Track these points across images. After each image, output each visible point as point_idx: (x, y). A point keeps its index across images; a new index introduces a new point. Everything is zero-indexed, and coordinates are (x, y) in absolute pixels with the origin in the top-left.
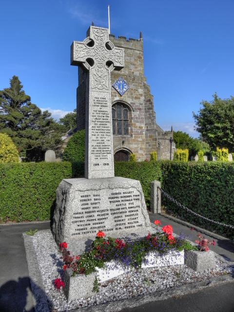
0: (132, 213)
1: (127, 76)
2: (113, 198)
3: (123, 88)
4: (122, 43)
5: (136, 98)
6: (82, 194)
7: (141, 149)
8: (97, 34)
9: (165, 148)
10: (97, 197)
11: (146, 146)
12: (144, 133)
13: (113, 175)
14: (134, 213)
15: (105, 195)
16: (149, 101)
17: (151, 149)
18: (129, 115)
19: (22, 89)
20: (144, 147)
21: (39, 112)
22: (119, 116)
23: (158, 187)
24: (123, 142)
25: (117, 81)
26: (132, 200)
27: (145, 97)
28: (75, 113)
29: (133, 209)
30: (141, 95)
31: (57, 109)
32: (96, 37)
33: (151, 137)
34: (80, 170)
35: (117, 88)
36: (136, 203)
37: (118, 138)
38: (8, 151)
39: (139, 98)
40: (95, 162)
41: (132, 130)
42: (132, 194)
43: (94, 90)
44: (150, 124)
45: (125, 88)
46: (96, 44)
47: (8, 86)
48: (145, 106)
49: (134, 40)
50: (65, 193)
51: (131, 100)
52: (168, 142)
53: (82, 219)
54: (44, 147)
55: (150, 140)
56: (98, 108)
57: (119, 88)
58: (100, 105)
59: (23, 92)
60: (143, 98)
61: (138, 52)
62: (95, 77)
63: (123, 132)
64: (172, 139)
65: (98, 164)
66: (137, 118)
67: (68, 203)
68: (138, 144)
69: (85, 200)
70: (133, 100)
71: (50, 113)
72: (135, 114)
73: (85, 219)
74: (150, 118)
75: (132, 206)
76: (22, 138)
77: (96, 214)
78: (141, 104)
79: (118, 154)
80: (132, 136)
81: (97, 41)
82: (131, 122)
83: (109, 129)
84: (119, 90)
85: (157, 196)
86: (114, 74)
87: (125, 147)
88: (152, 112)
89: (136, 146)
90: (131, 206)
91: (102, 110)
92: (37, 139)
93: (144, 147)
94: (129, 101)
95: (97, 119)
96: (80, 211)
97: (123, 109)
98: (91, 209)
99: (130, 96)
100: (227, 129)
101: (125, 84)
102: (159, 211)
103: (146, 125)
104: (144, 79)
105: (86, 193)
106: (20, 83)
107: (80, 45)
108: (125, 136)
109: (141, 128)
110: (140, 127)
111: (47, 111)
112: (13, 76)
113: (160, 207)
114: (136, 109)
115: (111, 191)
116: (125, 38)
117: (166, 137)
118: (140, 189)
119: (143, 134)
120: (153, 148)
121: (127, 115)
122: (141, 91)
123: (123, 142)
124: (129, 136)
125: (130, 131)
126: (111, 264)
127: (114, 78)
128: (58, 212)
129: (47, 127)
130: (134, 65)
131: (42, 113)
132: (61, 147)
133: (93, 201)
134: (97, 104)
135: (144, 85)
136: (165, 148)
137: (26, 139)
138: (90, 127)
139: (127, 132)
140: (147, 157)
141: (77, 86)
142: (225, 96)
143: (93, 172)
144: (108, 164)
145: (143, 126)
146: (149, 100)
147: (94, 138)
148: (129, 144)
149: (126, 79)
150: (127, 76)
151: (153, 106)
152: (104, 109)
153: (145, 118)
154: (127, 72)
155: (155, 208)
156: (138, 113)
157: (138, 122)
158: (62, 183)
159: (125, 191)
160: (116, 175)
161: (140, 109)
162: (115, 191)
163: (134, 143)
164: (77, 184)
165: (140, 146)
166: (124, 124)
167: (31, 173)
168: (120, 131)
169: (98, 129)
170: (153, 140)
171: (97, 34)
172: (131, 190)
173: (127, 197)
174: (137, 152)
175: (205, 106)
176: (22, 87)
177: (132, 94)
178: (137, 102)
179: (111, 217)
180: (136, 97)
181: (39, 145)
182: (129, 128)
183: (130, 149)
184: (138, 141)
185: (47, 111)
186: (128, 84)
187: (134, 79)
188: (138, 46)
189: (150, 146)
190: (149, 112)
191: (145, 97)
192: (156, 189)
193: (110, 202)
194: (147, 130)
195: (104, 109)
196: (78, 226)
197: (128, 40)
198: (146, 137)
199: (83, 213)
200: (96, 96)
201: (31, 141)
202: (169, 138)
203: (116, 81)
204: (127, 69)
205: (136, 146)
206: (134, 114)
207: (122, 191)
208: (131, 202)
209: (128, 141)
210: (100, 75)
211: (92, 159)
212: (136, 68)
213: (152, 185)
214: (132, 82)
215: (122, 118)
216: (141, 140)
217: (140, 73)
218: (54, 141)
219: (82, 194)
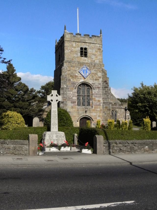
1: (89, 64)
2: (57, 136)
3: (86, 73)
4: (87, 39)
5: (96, 80)
6: (49, 135)
7: (99, 116)
9: (121, 115)
11: (103, 114)
12: (101, 105)
13: (58, 131)
15: (55, 136)
16: (106, 82)
17: (106, 116)
18: (90, 92)
20: (101, 115)
21: (28, 89)
22: (84, 92)
23: (76, 136)
24: (86, 112)
25: (82, 68)
27: (103, 78)
28: (54, 81)
30: (100, 77)
31: (36, 74)
33: (106, 108)
34: (49, 129)
35: (82, 73)
36: (63, 138)
37: (83, 108)
38: (21, 121)
39: (99, 80)
40: (53, 127)
41: (92, 102)
42: (62, 136)
44: (106, 99)
45: (88, 73)
46: (53, 95)
48: (103, 86)
49: (95, 36)
50: (45, 135)
51: (92, 81)
52: (123, 110)
54: (32, 113)
55: (106, 110)
56: (54, 113)
57: (84, 73)
59: (16, 74)
60: (101, 80)
61: (99, 45)
63: (86, 105)
64: (127, 108)
66: (96, 94)
67: (46, 137)
68: (97, 113)
69: (50, 136)
70: (93, 81)
71: (35, 90)
72: (95, 91)
74: (106, 94)
76: (16, 108)
77: (52, 140)
78: (100, 84)
79: (83, 119)
80: (92, 107)
82: (92, 97)
84: (83, 75)
85: (76, 139)
86: (80, 63)
87: (87, 115)
88: (108, 89)
89: (95, 114)
92: (26, 109)
93: (101, 115)
94: (90, 82)
96: (48, 139)
97: (86, 88)
98: (51, 139)
99: (92, 78)
100: (147, 107)
101: (88, 70)
102: (77, 144)
103: (103, 99)
104: (102, 65)
105: (50, 135)
106: (14, 68)
107: (49, 96)
108: (87, 107)
109: (99, 101)
110: (98, 101)
111: (33, 89)
113: (77, 143)
114: (96, 88)
115: (56, 135)
116: (89, 35)
117: (122, 107)
118: (64, 134)
119: (100, 106)
120: (107, 116)
121: (89, 91)
122: (100, 74)
123: (86, 112)
124: (90, 107)
125: (91, 103)
126: (53, 148)
127: (80, 65)
128: (43, 140)
129: (33, 100)
130: (95, 55)
131: (30, 90)
132: (42, 114)
133: (52, 137)
135: (102, 70)
136: (121, 115)
137: (19, 109)
138: (52, 118)
139: (89, 104)
140: (103, 122)
141: (54, 69)
142: (150, 83)
145: (101, 100)
146: (106, 81)
147: (53, 121)
148: (90, 112)
149: (89, 66)
150: (89, 64)
151: (109, 85)
152: (55, 113)
153: (103, 95)
154: (90, 61)
155: (75, 143)
156: (97, 90)
157: (97, 96)
158: (44, 133)
159: (60, 135)
160: (58, 131)
161: (99, 88)
162: (57, 135)
163: (94, 112)
164: (48, 133)
165: (98, 114)
166: (87, 98)
167: (35, 130)
168: (84, 103)
170: (108, 110)
172: (62, 135)
173: (60, 136)
174: (96, 118)
175: (134, 90)
177: (93, 77)
178: (97, 83)
179: (56, 141)
180: (96, 79)
181: (28, 113)
182: (91, 101)
183: (91, 117)
184: (96, 110)
185: (33, 89)
186: (90, 70)
187: (94, 66)
188: (98, 41)
189: (105, 114)
190: (105, 90)
191: (103, 79)
192: (75, 137)
194: (104, 103)
195: (55, 113)
197: (91, 37)
198: (103, 108)
200: (53, 110)
201: (22, 110)
202: (124, 107)
203: (81, 68)
204: (90, 58)
205: (95, 114)
206: (94, 91)
207: (59, 135)
209: (90, 110)
211: (52, 126)
212: (97, 57)
213: (74, 135)
214: (94, 68)
215: (86, 94)
216: (99, 110)
217: (99, 61)
218: (38, 110)
219: (49, 135)
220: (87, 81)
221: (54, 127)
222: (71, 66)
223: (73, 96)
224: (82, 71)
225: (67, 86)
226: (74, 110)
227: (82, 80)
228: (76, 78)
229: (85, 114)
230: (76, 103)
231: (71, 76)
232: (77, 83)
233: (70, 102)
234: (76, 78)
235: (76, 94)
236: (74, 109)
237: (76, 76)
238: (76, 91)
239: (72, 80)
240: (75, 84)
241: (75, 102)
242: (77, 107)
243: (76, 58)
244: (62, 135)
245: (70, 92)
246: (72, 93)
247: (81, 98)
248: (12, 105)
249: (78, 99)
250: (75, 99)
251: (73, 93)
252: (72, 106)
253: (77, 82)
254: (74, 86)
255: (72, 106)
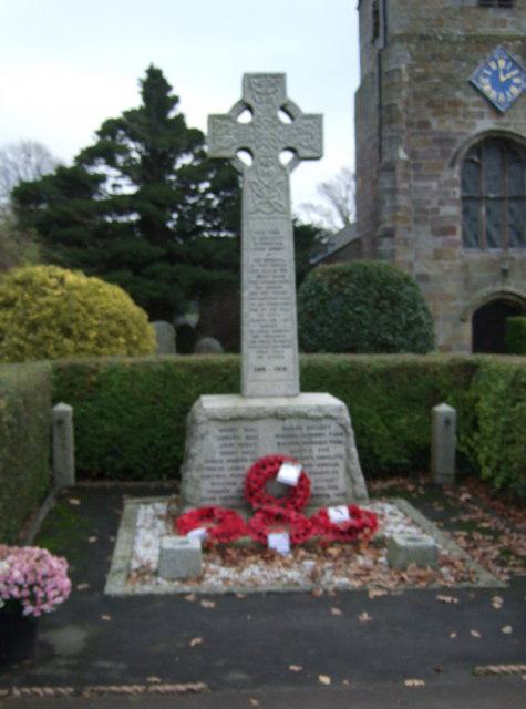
0: (325, 469)
8: (259, 90)
10: (251, 434)
14: (330, 469)
19: (97, 308)
26: (325, 442)
29: (327, 461)
32: (257, 97)
42: (326, 432)
43: (254, 216)
47: (137, 102)
53: (221, 473)
56: (263, 255)
58: (267, 247)
59: (180, 118)
62: (255, 188)
65: (264, 369)
73: (226, 473)
75: (325, 454)
81: (260, 107)
83: (288, 295)
90: (322, 454)
91: (271, 257)
95: (260, 276)
96: (218, 457)
98: (240, 456)
112: (147, 67)
123: (505, 273)
134: (261, 246)
141: (354, 82)
143: (253, 384)
144: (285, 369)
147: (254, 315)
152: (278, 255)
169: (263, 296)
171: (259, 90)
176: (175, 100)
193: (279, 444)
195: (278, 255)
196: (213, 484)
199: (221, 461)
208: (325, 446)
210: (266, 182)
220: (509, 124)
221: (271, 364)
222: (434, 57)
223: (441, 203)
224: (486, 76)
225: (413, 154)
226: (447, 268)
227: (487, 124)
228: (456, 114)
229: (499, 288)
230: (458, 237)
231: (431, 104)
232: (461, 140)
233: (428, 228)
234: (456, 114)
235: (458, 192)
236: (446, 264)
237: (455, 104)
238: (456, 176)
239: (435, 124)
240: (452, 142)
241: (452, 231)
242: (460, 250)
243: (456, 14)
244: (325, 422)
245: (427, 184)
246: (434, 185)
247: (483, 211)
248: (159, 251)
249: (466, 212)
250: (454, 217)
251: (440, 185)
252: (436, 251)
253: (461, 133)
254: (444, 154)
255: (436, 251)
